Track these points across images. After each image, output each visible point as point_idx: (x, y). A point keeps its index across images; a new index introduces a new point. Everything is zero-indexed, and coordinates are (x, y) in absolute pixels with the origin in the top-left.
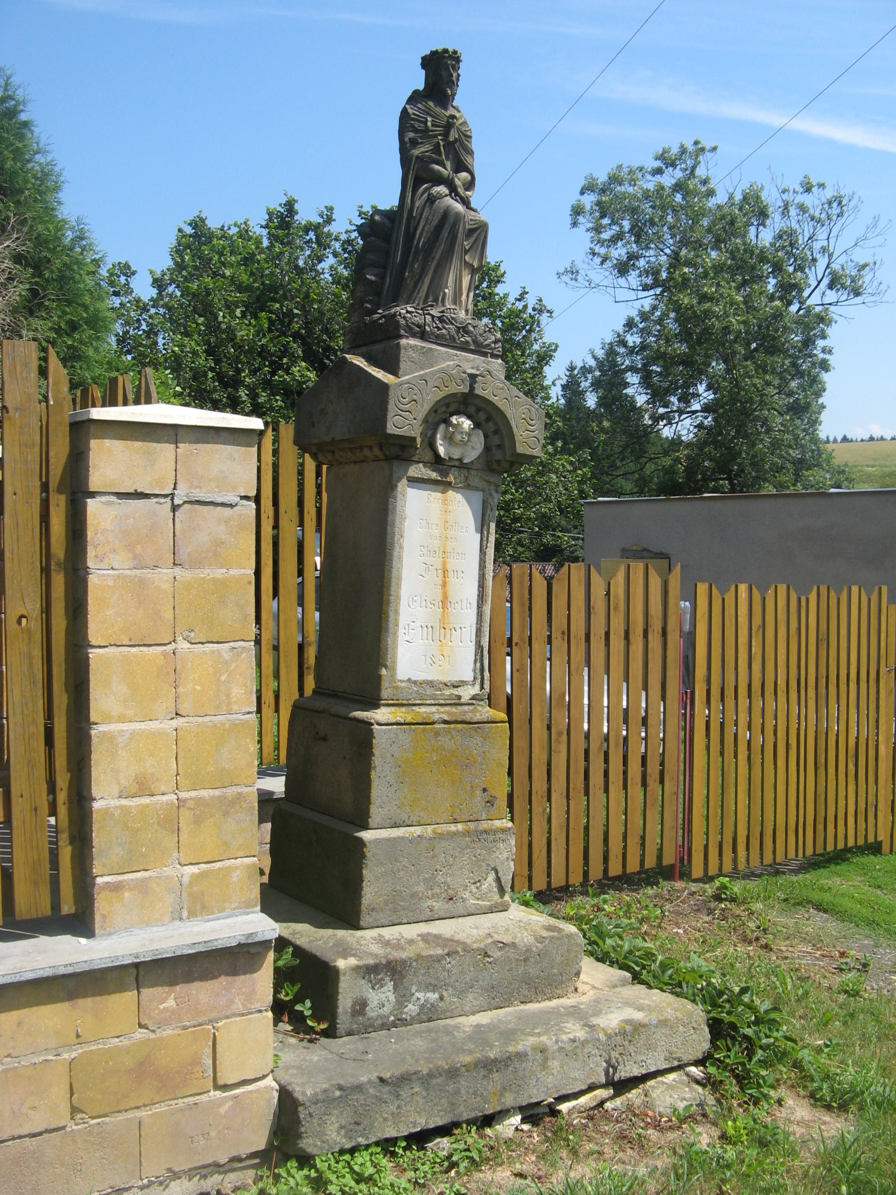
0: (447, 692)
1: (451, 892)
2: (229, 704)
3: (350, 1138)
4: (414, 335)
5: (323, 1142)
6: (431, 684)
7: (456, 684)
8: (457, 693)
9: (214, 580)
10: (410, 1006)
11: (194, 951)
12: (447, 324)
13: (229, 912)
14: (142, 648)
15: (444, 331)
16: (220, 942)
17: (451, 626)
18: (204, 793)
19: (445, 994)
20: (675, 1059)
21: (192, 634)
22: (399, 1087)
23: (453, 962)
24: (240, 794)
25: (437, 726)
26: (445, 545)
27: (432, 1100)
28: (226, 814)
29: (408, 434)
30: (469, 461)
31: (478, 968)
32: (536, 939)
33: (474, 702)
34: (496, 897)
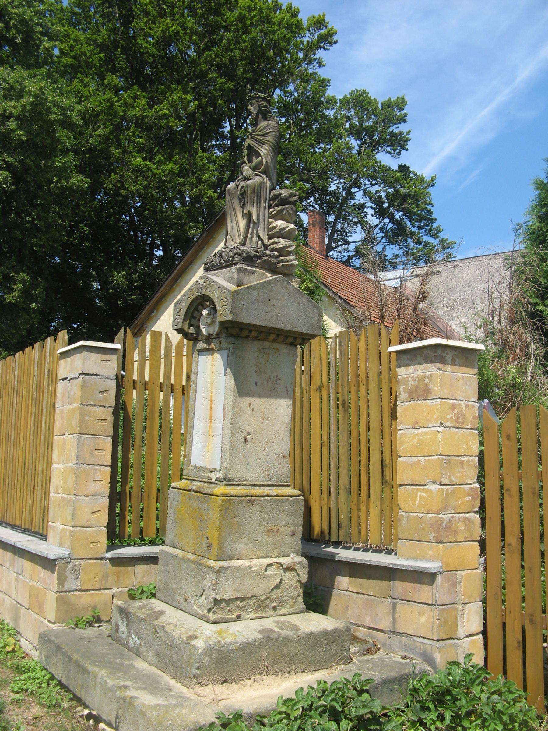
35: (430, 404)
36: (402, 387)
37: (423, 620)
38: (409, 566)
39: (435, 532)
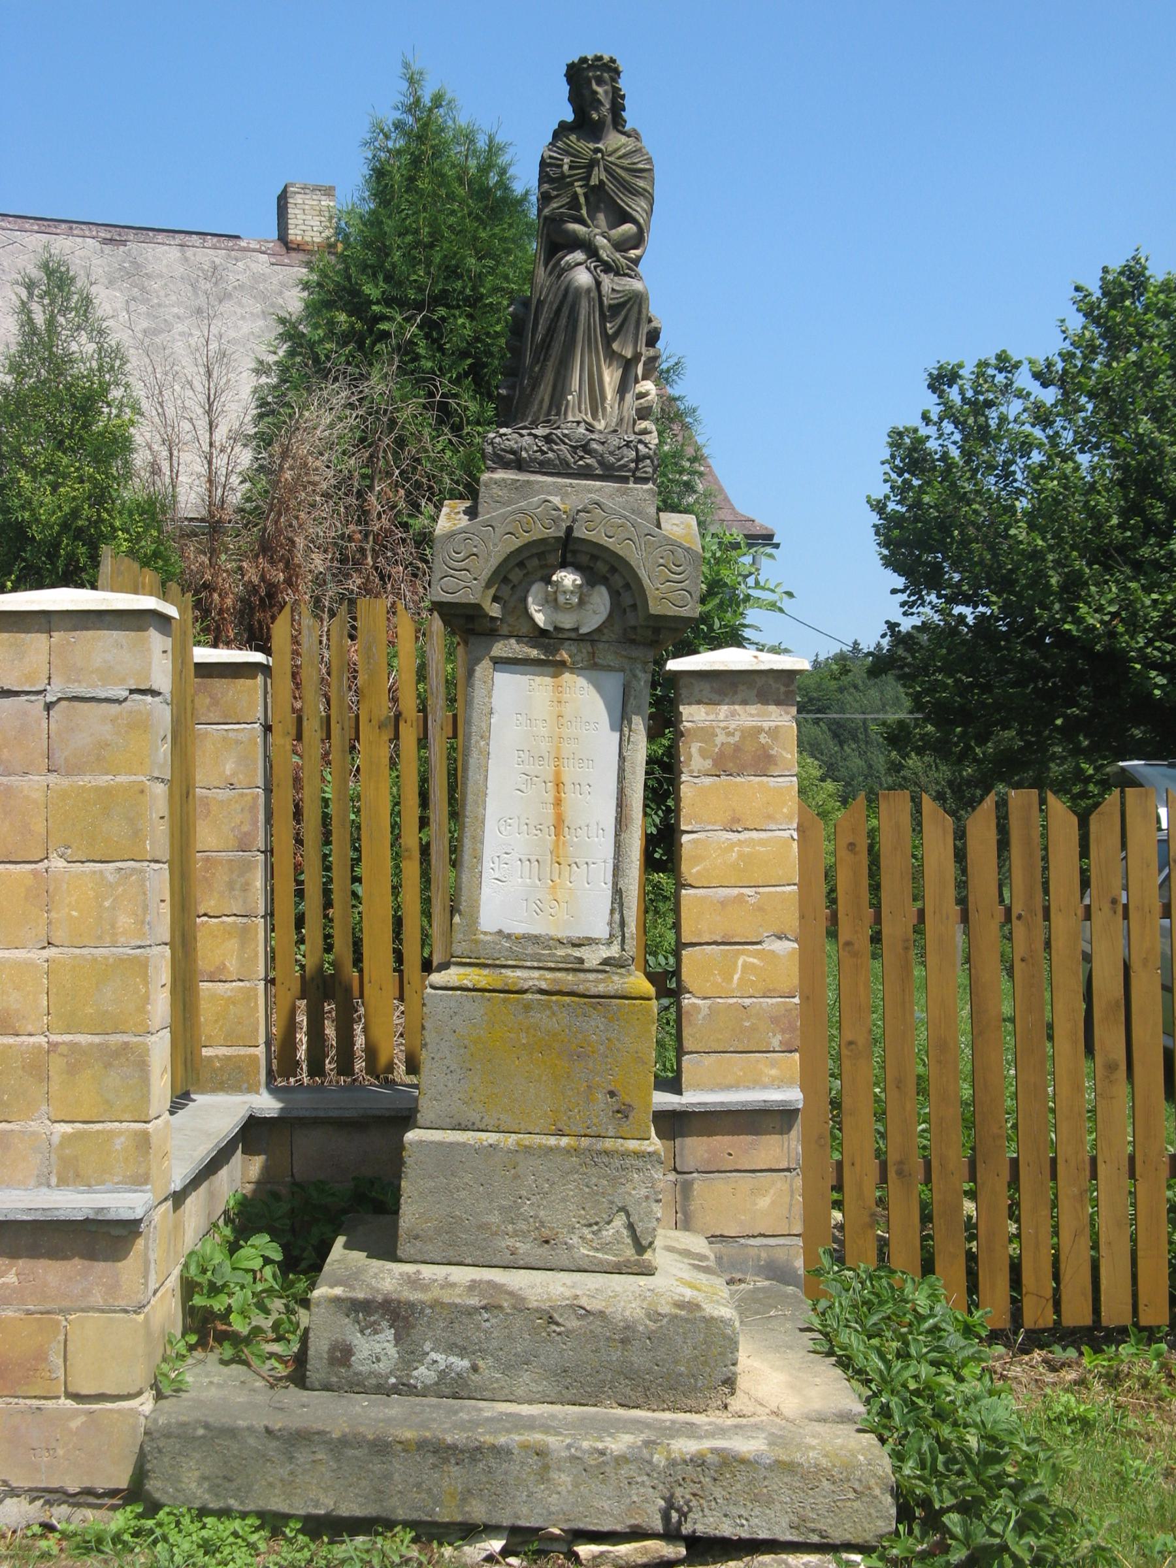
0: (561, 952)
1: (546, 1232)
2: (114, 935)
3: (217, 1495)
4: (506, 465)
5: (177, 1490)
6: (535, 939)
7: (577, 942)
8: (578, 954)
9: (97, 789)
10: (422, 1369)
11: (29, 1218)
12: (557, 444)
13: (109, 1186)
14: (8, 866)
15: (551, 455)
16: (62, 1212)
17: (571, 861)
18: (83, 1039)
19: (481, 1363)
20: (813, 1531)
21: (69, 851)
22: (293, 1445)
23: (494, 1321)
24: (126, 1044)
25: (529, 996)
26: (559, 748)
27: (345, 1478)
28: (108, 1065)
29: (464, 601)
30: (589, 630)
31: (538, 1338)
32: (648, 1316)
33: (608, 968)
34: (630, 1253)
35: (771, 784)
36: (695, 748)
37: (764, 1203)
38: (737, 1103)
39: (783, 1032)
